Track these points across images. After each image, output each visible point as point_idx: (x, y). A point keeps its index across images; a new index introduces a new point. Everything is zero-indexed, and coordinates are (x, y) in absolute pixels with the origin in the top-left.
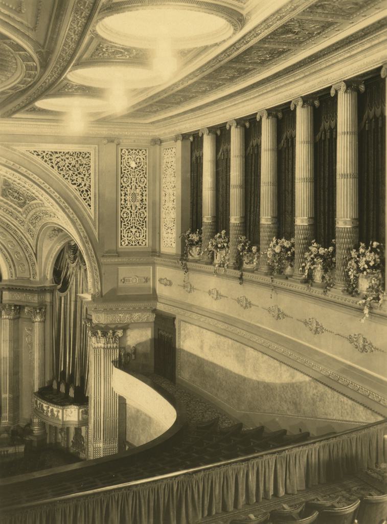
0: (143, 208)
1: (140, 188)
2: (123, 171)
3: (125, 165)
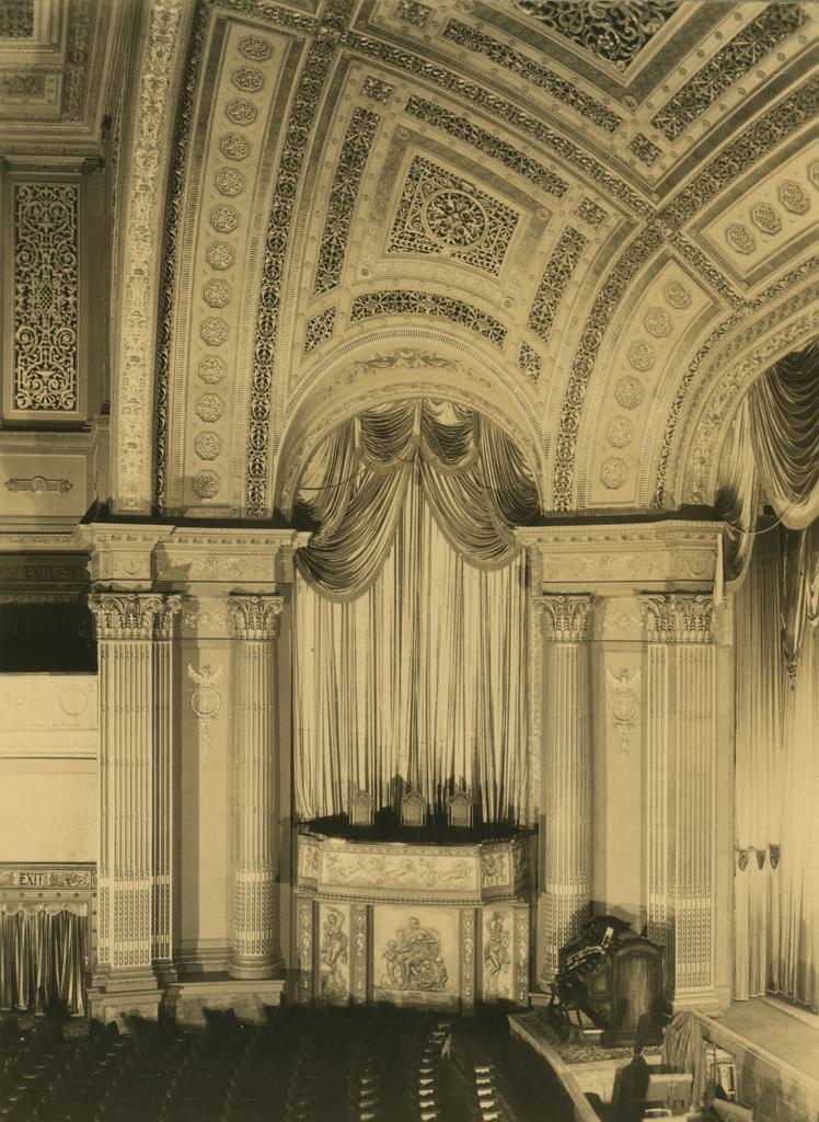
0: (23, 274)
1: (60, 275)
2: (21, 237)
3: (25, 222)
